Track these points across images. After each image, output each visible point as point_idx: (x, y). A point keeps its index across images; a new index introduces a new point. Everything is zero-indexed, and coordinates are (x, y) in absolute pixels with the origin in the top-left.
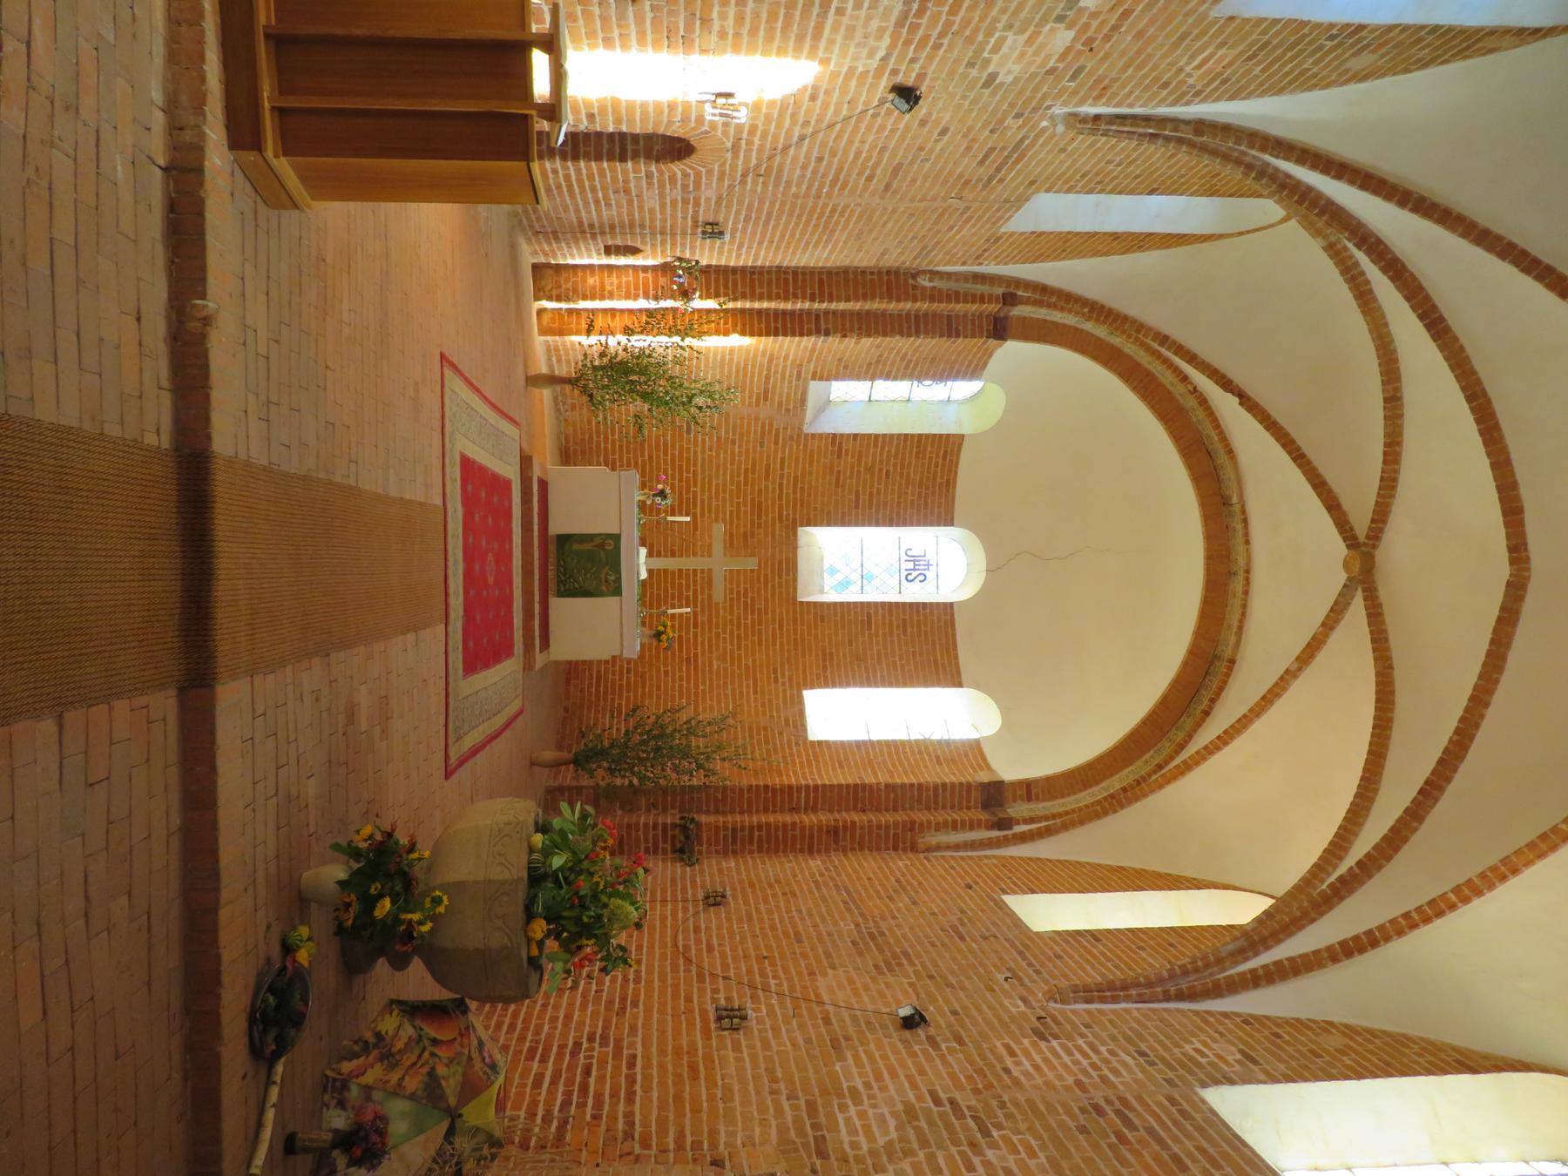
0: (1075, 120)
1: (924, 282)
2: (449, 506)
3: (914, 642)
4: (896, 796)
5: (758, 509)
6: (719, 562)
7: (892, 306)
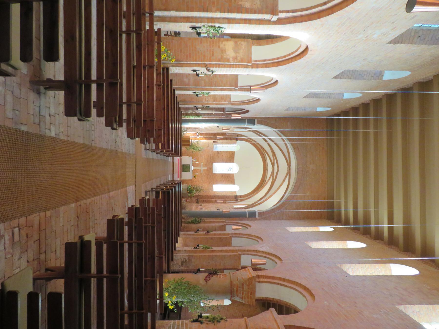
2: (219, 219)
3: (229, 178)
5: (208, 161)
6: (202, 168)
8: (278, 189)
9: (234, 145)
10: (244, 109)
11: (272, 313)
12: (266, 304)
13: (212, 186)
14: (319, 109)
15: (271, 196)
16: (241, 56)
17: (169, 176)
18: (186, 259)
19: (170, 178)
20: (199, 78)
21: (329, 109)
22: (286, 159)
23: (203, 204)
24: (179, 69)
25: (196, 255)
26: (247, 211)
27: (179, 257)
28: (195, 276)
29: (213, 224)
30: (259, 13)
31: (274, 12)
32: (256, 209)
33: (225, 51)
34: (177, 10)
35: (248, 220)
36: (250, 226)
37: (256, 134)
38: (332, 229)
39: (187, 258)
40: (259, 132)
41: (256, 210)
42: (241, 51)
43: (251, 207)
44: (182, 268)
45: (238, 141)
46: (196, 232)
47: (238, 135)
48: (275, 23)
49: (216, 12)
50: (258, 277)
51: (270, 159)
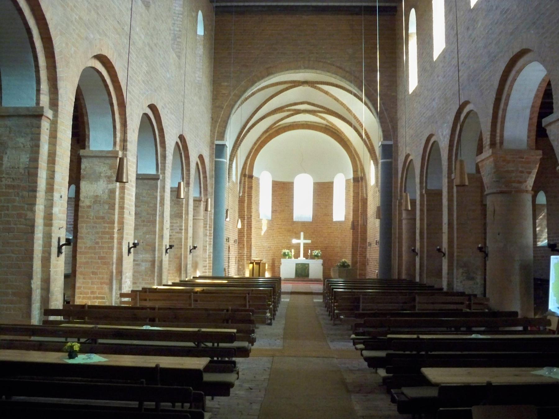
0: (229, 182)
1: (241, 195)
3: (323, 192)
4: (356, 202)
7: (246, 201)
8: (342, 104)
9: (261, 182)
10: (197, 164)
11: (550, 124)
12: (540, 134)
13: (336, 222)
14: (200, 31)
15: (355, 117)
16: (105, 169)
17: (315, 300)
18: (463, 273)
19: (319, 300)
20: (141, 244)
21: (200, 14)
22: (287, 89)
23: (368, 241)
24: (126, 277)
25: (455, 254)
26: (380, 161)
27: (459, 284)
28: (490, 255)
29: (404, 222)
30: (39, 139)
31: (37, 115)
32: (377, 142)
33: (97, 196)
34: (30, 276)
35: (396, 160)
36: (407, 156)
37: (241, 141)
38: (413, 12)
39: (461, 270)
40: (238, 137)
41: (380, 144)
42: (98, 169)
43: (375, 153)
44: (479, 279)
45: (255, 174)
46: (417, 254)
47: (243, 175)
48: (56, 115)
49: (33, 212)
50: (493, 144)
51: (288, 116)
